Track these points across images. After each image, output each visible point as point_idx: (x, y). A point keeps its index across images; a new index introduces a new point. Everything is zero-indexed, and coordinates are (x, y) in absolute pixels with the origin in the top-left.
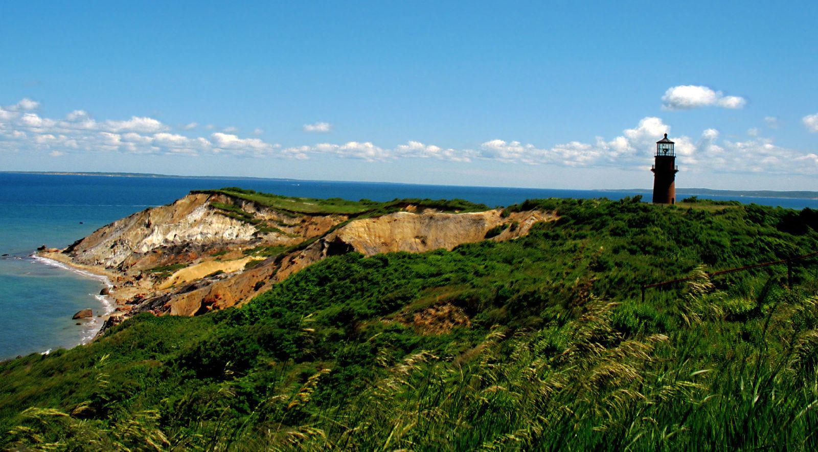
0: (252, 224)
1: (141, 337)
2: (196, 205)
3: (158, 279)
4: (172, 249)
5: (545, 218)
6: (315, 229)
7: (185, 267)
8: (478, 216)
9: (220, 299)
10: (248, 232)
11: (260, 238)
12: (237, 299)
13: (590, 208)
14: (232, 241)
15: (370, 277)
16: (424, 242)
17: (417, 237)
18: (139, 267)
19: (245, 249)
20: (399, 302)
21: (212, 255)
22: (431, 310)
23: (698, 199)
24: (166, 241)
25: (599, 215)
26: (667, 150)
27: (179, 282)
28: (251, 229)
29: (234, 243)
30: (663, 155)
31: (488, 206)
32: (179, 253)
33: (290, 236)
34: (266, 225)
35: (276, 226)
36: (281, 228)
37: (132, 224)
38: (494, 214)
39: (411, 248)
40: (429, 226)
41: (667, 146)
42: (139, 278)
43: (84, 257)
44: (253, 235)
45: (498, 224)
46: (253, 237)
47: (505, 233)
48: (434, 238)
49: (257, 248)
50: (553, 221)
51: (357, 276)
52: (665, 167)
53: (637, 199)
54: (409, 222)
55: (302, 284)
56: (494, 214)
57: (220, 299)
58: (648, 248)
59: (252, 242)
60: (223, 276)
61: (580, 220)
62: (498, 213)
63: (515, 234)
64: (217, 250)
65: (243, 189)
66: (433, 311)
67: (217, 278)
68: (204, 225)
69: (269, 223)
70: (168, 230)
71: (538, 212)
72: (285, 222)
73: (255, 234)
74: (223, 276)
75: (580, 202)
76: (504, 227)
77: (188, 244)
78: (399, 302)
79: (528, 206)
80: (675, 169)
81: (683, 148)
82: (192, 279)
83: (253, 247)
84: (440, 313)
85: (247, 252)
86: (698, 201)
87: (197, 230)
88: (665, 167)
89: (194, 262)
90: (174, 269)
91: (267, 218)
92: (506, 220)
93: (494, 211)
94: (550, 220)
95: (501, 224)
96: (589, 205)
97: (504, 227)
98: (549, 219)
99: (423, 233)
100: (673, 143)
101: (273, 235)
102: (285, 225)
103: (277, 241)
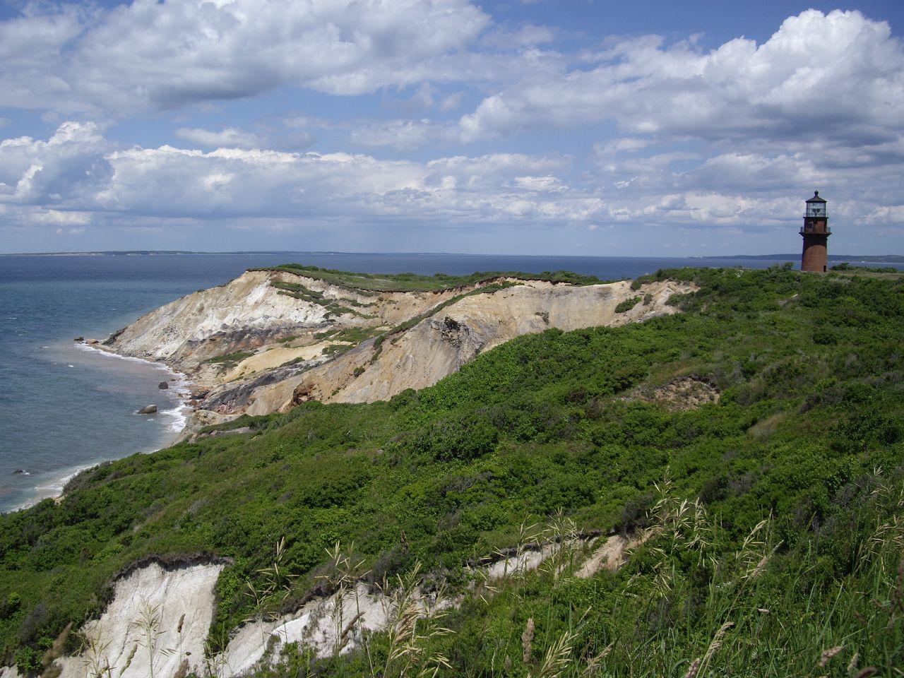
0: (322, 304)
1: (316, 427)
2: (254, 285)
3: (223, 370)
4: (232, 335)
5: (683, 290)
6: (394, 308)
7: (250, 356)
8: (604, 288)
9: (315, 389)
10: (317, 315)
11: (333, 320)
12: (334, 388)
13: (733, 278)
14: (300, 325)
15: (579, 355)
16: (546, 320)
17: (537, 314)
18: (196, 357)
19: (315, 333)
20: (631, 379)
21: (279, 341)
22: (672, 386)
23: (848, 266)
24: (225, 326)
25: (745, 285)
26: (818, 210)
27: (247, 372)
28: (320, 310)
29: (302, 327)
30: (814, 216)
31: (600, 279)
32: (239, 341)
33: (365, 317)
34: (337, 306)
35: (349, 306)
36: (355, 309)
37: (181, 310)
38: (623, 285)
39: (532, 325)
40: (549, 300)
41: (818, 206)
42: (198, 369)
43: (130, 348)
44: (324, 316)
45: (628, 298)
46: (324, 319)
47: (638, 307)
48: (557, 313)
49: (330, 333)
50: (692, 294)
51: (562, 354)
52: (815, 232)
53: (787, 268)
54: (528, 297)
55: (498, 364)
56: (623, 285)
57: (315, 389)
58: (851, 321)
59: (323, 325)
60: (303, 363)
61: (723, 291)
62: (628, 285)
63: (649, 309)
64: (287, 335)
65: (304, 266)
66: (674, 388)
67: (296, 367)
68: (261, 304)
69: (340, 303)
70: (224, 315)
71: (675, 283)
72: (359, 301)
73: (326, 316)
74: (303, 363)
75: (721, 271)
76: (636, 300)
77: (250, 330)
78: (631, 379)
79: (660, 276)
80: (828, 231)
81: (835, 210)
82: (263, 368)
83: (324, 331)
84: (683, 389)
85: (320, 337)
86: (849, 269)
87: (258, 313)
88: (815, 232)
89: (259, 349)
90: (240, 356)
91: (338, 297)
92: (637, 293)
93: (623, 282)
94: (688, 292)
95: (632, 298)
96: (731, 275)
97: (636, 300)
98: (687, 290)
99: (544, 310)
100: (825, 202)
101: (346, 317)
102: (359, 305)
103: (351, 323)
